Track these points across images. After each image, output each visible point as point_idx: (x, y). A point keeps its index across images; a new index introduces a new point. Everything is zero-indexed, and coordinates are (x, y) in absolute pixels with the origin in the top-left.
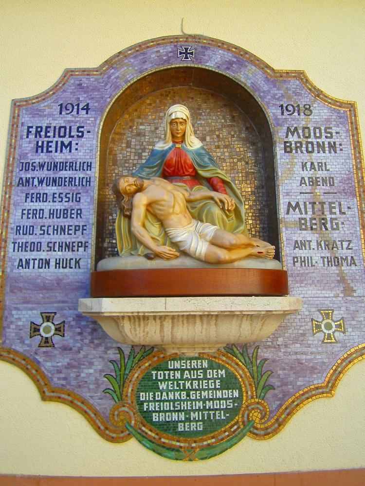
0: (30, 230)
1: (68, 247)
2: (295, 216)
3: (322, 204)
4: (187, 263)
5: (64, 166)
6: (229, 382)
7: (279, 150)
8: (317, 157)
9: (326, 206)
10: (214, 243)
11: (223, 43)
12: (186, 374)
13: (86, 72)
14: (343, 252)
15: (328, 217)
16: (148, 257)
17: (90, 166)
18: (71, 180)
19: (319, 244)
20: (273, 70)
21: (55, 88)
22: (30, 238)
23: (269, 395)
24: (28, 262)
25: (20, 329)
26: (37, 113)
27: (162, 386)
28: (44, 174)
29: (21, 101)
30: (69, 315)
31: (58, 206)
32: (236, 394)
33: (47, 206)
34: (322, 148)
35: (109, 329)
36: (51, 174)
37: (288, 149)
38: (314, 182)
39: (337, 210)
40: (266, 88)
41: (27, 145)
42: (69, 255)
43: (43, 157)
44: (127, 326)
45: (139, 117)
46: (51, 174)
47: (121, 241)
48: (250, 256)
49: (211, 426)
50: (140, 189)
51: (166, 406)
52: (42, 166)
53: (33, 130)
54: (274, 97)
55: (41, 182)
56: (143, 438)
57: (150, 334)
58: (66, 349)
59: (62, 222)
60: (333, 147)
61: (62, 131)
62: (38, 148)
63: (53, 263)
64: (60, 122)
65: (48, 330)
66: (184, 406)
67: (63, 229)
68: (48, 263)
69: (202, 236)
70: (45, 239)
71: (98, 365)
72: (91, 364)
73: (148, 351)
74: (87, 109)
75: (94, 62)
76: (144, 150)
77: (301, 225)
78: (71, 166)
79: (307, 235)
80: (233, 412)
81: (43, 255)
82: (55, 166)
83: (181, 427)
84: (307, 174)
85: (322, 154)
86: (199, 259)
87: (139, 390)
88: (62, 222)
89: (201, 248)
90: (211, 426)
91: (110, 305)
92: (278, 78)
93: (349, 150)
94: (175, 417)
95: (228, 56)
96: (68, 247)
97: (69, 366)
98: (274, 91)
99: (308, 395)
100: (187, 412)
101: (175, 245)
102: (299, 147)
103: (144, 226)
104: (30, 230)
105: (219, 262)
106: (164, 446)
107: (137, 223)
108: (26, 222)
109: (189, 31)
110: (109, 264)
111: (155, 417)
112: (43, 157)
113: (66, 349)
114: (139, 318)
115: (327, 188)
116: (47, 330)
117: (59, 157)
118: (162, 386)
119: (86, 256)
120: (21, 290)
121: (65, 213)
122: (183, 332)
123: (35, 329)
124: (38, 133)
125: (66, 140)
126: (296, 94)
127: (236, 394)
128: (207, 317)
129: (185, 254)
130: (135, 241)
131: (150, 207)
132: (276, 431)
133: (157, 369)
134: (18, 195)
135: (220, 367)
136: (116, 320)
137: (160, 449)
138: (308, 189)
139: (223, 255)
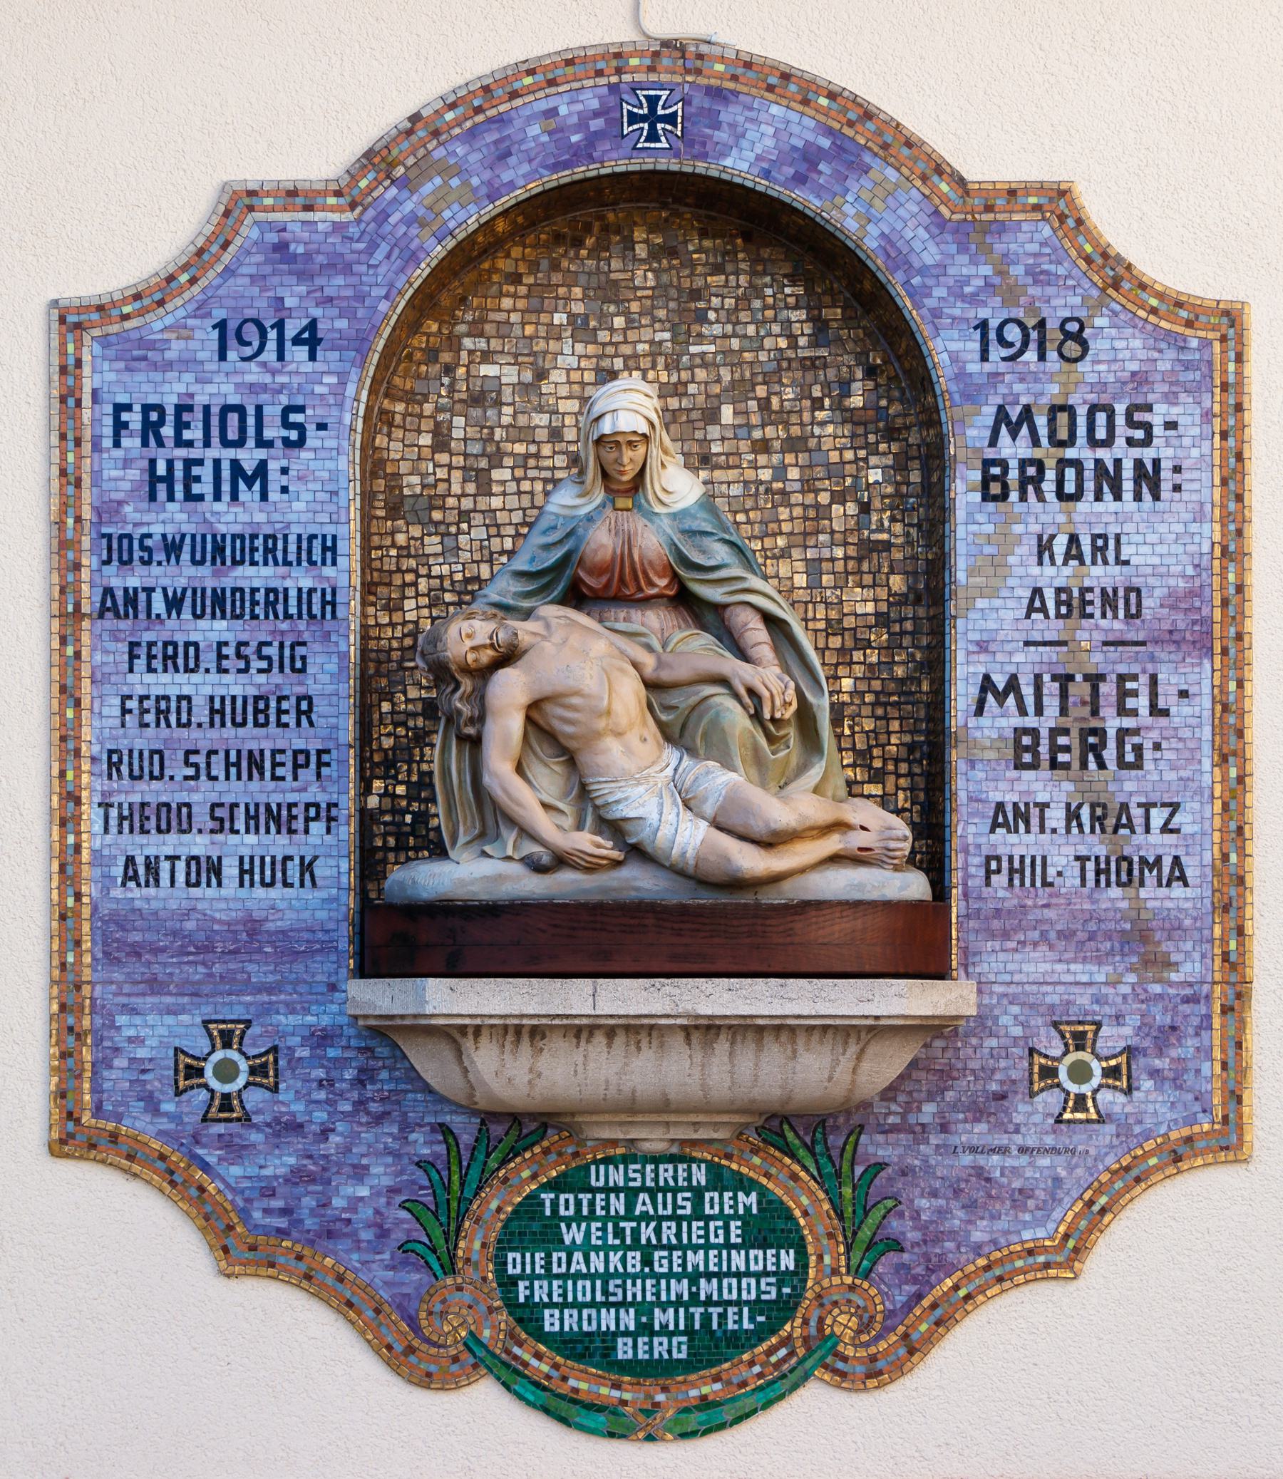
3: (1095, 680)
12: (643, 1204)
14: (1153, 843)
15: (1112, 724)
16: (538, 868)
17: (331, 549)
18: (274, 597)
19: (1072, 815)
20: (961, 182)
24: (152, 867)
27: (572, 1235)
28: (183, 575)
31: (235, 686)
32: (788, 1260)
34: (1109, 479)
36: (206, 577)
39: (1142, 703)
42: (279, 844)
45: (476, 330)
46: (206, 577)
50: (508, 656)
52: (172, 548)
53: (134, 419)
55: (174, 604)
59: (251, 738)
60: (1148, 478)
63: (230, 870)
67: (255, 762)
68: (215, 869)
70: (201, 796)
76: (496, 459)
81: (199, 844)
83: (624, 1350)
84: (1054, 575)
86: (678, 871)
88: (251, 738)
94: (608, 1320)
95: (804, 130)
97: (297, 1177)
98: (961, 266)
100: (644, 1309)
101: (614, 828)
102: (1031, 479)
103: (520, 770)
105: (737, 884)
106: (574, 1400)
108: (144, 741)
111: (551, 1321)
115: (1116, 626)
116: (226, 1071)
118: (572, 1235)
124: (150, 430)
125: (249, 457)
126: (1038, 276)
127: (788, 1260)
129: (638, 853)
132: (899, 1369)
133: (556, 1186)
135: (745, 1185)
139: (751, 861)
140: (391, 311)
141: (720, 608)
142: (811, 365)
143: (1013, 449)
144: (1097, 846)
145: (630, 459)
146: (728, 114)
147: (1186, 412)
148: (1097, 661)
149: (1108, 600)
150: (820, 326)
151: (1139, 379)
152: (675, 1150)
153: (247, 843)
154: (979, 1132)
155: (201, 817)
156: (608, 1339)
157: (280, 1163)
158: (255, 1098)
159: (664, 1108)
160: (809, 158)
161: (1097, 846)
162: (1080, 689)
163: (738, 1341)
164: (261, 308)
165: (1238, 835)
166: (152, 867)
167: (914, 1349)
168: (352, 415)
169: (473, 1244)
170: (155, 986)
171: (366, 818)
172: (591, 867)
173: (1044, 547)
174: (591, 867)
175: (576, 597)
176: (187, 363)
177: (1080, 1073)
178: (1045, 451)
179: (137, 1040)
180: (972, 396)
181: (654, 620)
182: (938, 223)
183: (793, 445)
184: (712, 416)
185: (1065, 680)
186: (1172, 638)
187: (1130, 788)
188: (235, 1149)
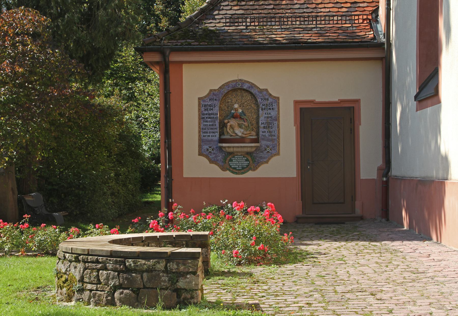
0: (205, 129)
1: (214, 133)
2: (263, 125)
3: (269, 123)
4: (238, 137)
5: (211, 114)
6: (247, 160)
7: (260, 110)
8: (269, 111)
9: (270, 123)
10: (243, 133)
11: (248, 82)
12: (238, 159)
13: (215, 90)
14: (273, 134)
15: (270, 126)
16: (230, 136)
17: (217, 114)
18: (213, 117)
19: (268, 132)
20: (260, 89)
21: (208, 94)
22: (205, 131)
23: (255, 163)
24: (205, 136)
25: (204, 149)
26: (204, 101)
27: (234, 161)
28: (207, 116)
29: (200, 98)
30: (215, 147)
31: (211, 124)
32: (248, 162)
33: (208, 124)
34: (270, 109)
35: (224, 149)
36: (209, 116)
37: (262, 110)
38: (268, 117)
39: (272, 124)
40: (258, 94)
41: (203, 109)
42: (214, 134)
43: (206, 112)
44: (227, 149)
45: (228, 98)
46: (209, 116)
47: (226, 133)
48: (250, 136)
49: (243, 168)
50: (229, 122)
51: (234, 164)
52: (206, 114)
53: (204, 105)
54: (260, 96)
55: (207, 118)
56: (230, 170)
57: (231, 150)
58: (214, 153)
59: (212, 127)
60: (273, 109)
61: (210, 106)
62: (205, 110)
63: (210, 136)
64: (210, 103)
65: (210, 150)
66: (238, 164)
67: (212, 129)
68: (209, 136)
69: (241, 132)
70: (208, 131)
71: (221, 157)
72: (219, 157)
73: (230, 153)
74: (216, 100)
75: (217, 88)
76: (229, 107)
77: (264, 127)
78: (213, 114)
79: (265, 130)
80: (247, 166)
81: (208, 134)
82: (209, 114)
83: (237, 169)
84: (266, 115)
85: (270, 111)
86: (240, 136)
87: (229, 161)
88: (212, 127)
89: (240, 134)
90: (243, 168)
91: (224, 145)
92: (261, 91)
93: (277, 109)
94: (236, 166)
95: (249, 85)
96: (214, 133)
97: (215, 157)
98: (260, 95)
99: (262, 163)
100: (238, 166)
101: (236, 134)
102: (265, 109)
103: (229, 130)
104: (205, 129)
105: (243, 137)
106: (234, 172)
107: (228, 130)
108: (205, 127)
109: (240, 78)
110: (223, 137)
111: (232, 167)
112: (206, 112)
113: (214, 153)
114: (229, 147)
115: (270, 119)
116: (210, 150)
117: (210, 112)
118: (234, 161)
119: (217, 135)
120: (204, 142)
121: (212, 125)
122: (235, 150)
123: (208, 150)
124: (205, 106)
125: (212, 108)
126: (265, 95)
127: (248, 162)
128: (241, 147)
129: (237, 135)
130: (228, 133)
131: (231, 126)
132: (256, 170)
133: (233, 157)
134: (202, 121)
135: (245, 157)
136: (225, 147)
137: (233, 172)
138: (266, 119)
139: (244, 136)
140: (221, 98)
141: (243, 119)
142: (251, 100)
143: (263, 107)
144: (269, 134)
145: (236, 109)
146: (244, 84)
147: (275, 104)
148: (269, 121)
149: (270, 117)
150: (252, 98)
151: (272, 102)
152: (423, 272)
153: (212, 134)
154: (262, 153)
155: (208, 132)
156: (236, 168)
157: (214, 156)
158: (212, 151)
159: (239, 152)
160: (250, 87)
161: (269, 134)
162: (268, 123)
163: (245, 168)
164: (212, 98)
165: (279, 133)
166: (205, 136)
167: (257, 168)
168: (219, 105)
169: (227, 161)
170: (205, 144)
171: (220, 132)
172: (234, 136)
173: (266, 114)
174: (234, 136)
175: (234, 118)
176: (207, 102)
177: (268, 149)
178: (266, 107)
179: (116, 212)
180: (261, 103)
181: (238, 119)
182: (258, 91)
183: (250, 106)
184: (244, 103)
185: (267, 123)
186: (274, 120)
187: (271, 130)
188: (211, 155)
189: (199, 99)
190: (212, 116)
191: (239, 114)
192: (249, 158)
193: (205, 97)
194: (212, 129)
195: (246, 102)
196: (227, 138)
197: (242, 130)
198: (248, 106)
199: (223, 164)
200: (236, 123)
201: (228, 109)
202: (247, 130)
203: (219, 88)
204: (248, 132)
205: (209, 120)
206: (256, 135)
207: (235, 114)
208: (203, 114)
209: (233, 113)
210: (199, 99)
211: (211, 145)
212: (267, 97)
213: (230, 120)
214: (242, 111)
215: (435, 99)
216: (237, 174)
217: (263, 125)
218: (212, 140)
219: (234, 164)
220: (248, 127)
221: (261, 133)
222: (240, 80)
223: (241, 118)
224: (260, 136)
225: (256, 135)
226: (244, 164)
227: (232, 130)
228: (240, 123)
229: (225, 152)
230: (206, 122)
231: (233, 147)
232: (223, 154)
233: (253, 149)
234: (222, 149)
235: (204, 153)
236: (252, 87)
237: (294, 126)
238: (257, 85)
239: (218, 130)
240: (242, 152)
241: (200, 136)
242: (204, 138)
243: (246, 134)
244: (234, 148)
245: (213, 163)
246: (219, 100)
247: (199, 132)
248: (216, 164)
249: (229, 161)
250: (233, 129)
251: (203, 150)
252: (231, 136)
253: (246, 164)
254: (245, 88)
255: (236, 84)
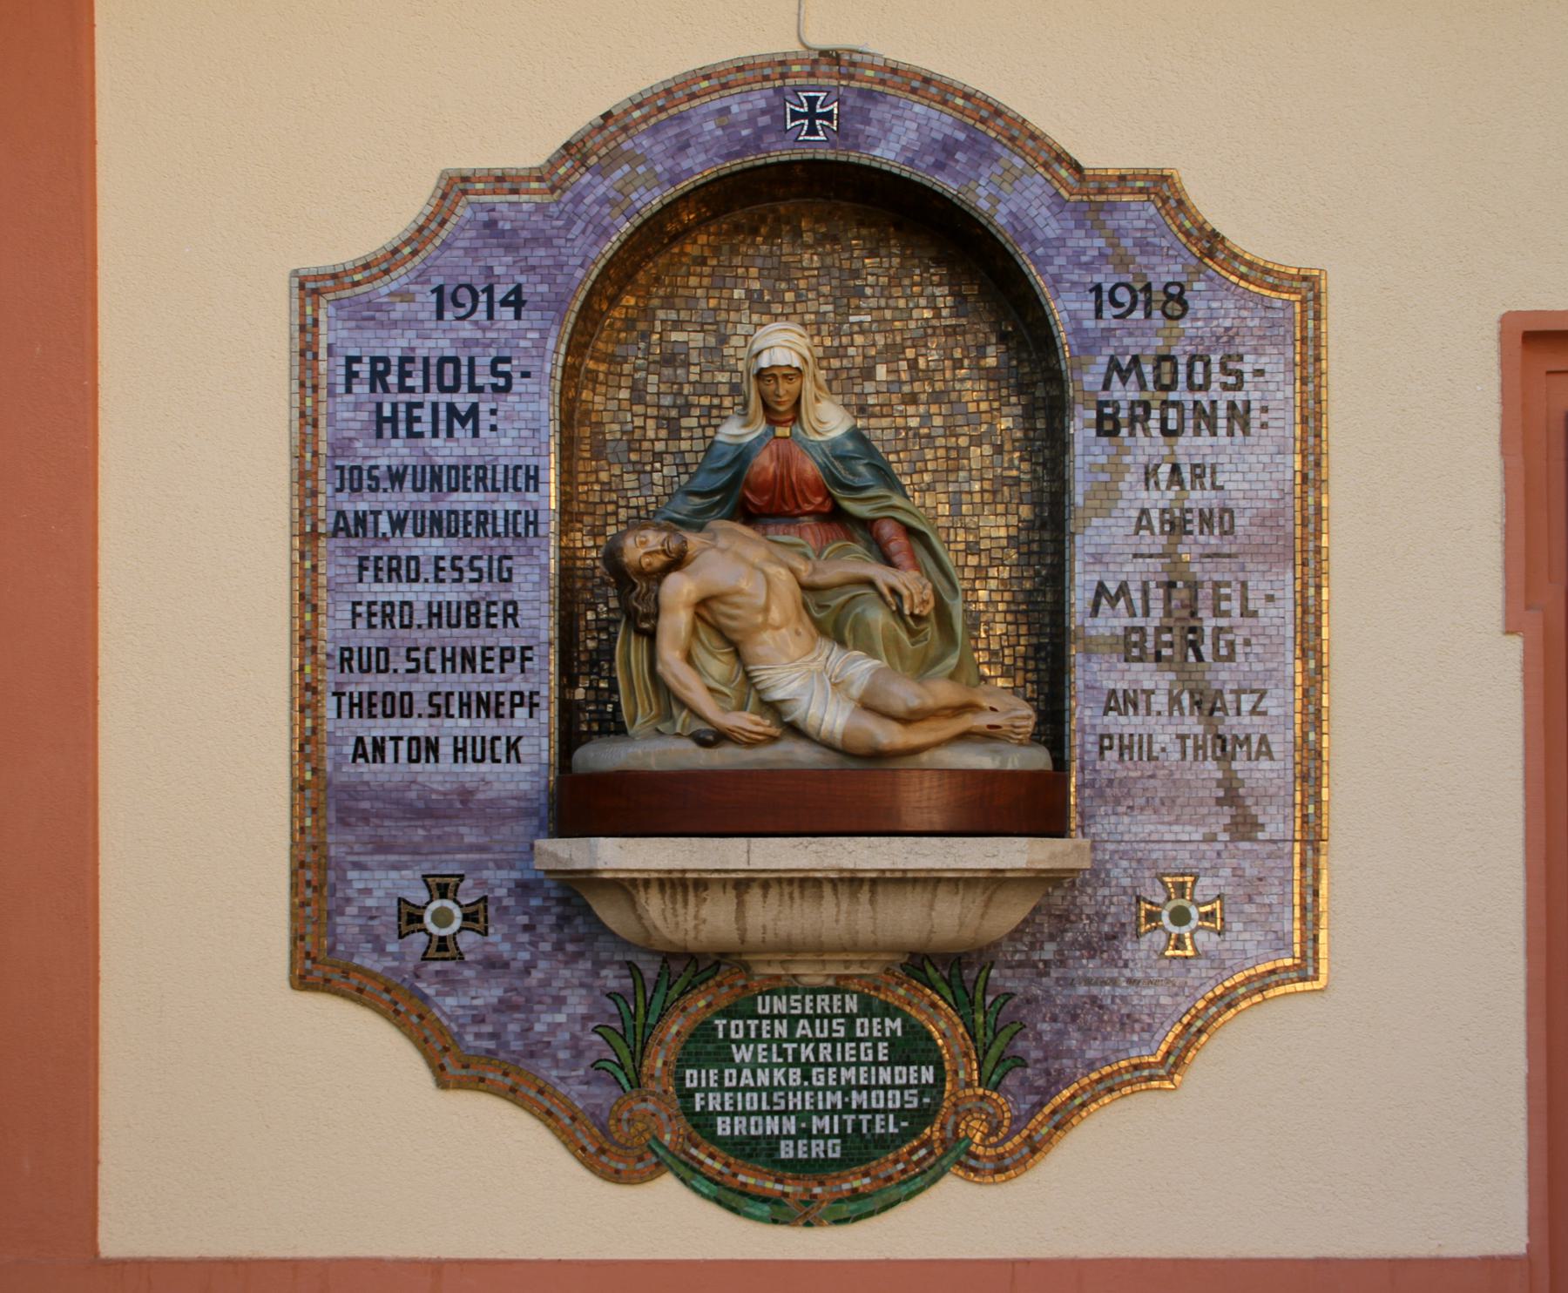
0: (377, 661)
1: (487, 705)
4: (800, 754)
7: (1080, 427)
8: (1192, 446)
9: (1206, 592)
10: (868, 706)
12: (803, 1028)
13: (503, 181)
16: (702, 742)
17: (534, 479)
19: (1174, 701)
20: (1077, 168)
21: (420, 235)
22: (380, 683)
24: (379, 746)
25: (369, 914)
26: (368, 315)
27: (742, 1054)
28: (404, 500)
30: (500, 881)
31: (451, 593)
32: (928, 1075)
33: (420, 594)
34: (1205, 418)
35: (611, 914)
36: (425, 501)
37: (1107, 425)
39: (1235, 607)
42: (487, 726)
43: (396, 452)
44: (654, 906)
45: (668, 302)
46: (425, 501)
47: (639, 709)
48: (965, 737)
50: (677, 561)
51: (751, 1101)
52: (397, 477)
53: (363, 369)
54: (1076, 261)
55: (398, 524)
56: (690, 1173)
58: (493, 965)
59: (464, 637)
63: (446, 749)
64: (438, 344)
66: (795, 1101)
68: (433, 747)
70: (421, 686)
71: (577, 1004)
72: (559, 1002)
74: (516, 301)
76: (685, 409)
77: (1130, 646)
78: (482, 477)
81: (419, 727)
82: (435, 478)
83: (786, 1151)
85: (1205, 439)
86: (827, 745)
87: (683, 1064)
88: (464, 637)
93: (1285, 424)
94: (772, 1125)
95: (943, 124)
96: (487, 705)
97: (505, 1006)
98: (1078, 239)
100: (803, 1116)
101: (773, 709)
103: (689, 658)
104: (377, 661)
105: (878, 756)
106: (743, 1192)
109: (821, 38)
111: (723, 1127)
112: (396, 452)
113: (493, 965)
114: (678, 885)
116: (443, 918)
117: (447, 451)
118: (742, 1054)
120: (365, 817)
124: (378, 378)
125: (463, 400)
126: (1143, 246)
127: (928, 1075)
128: (851, 882)
129: (795, 730)
130: (667, 697)
131: (704, 608)
132: (1022, 1164)
133: (728, 1014)
135: (889, 1011)
136: (626, 887)
137: (732, 1198)
139: (889, 735)
141: (867, 525)
142: (951, 331)
146: (878, 112)
149: (1206, 520)
151: (1230, 335)
153: (461, 726)
154: (1091, 966)
155: (421, 704)
156: (773, 1141)
157: (491, 994)
158: (468, 940)
159: (819, 950)
160: (948, 148)
163: (885, 1143)
165: (1314, 718)
166: (379, 746)
167: (1035, 1148)
169: (657, 1062)
170: (382, 847)
172: (751, 744)
175: (748, 515)
176: (409, 322)
180: (1088, 347)
181: (807, 535)
182: (1059, 203)
183: (936, 397)
184: (868, 374)
188: (449, 983)
189: (309, 288)
190: (468, 500)
191: (810, 468)
192: (943, 1027)
193: (389, 260)
194: (468, 658)
195: (892, 353)
196: (653, 764)
197: (861, 669)
198: (912, 399)
199: (603, 1095)
200: (781, 575)
201: (674, 433)
202: (923, 668)
203: (553, 164)
204: (942, 692)
205: (432, 546)
206: (1036, 738)
207: (765, 462)
208: (354, 479)
209: (742, 456)
210: (309, 288)
211: (449, 866)
212: (1163, 273)
213: (694, 540)
214: (855, 434)
215: (784, 707)
216: (779, 1212)
217: (1112, 622)
218: (464, 802)
219: (751, 1101)
220: (931, 629)
221: (1084, 715)
222: (831, 57)
223: (835, 517)
224: (1080, 744)
225: (1036, 738)
226: (878, 1100)
227: (718, 666)
228: (833, 572)
229: (627, 945)
230: (395, 569)
231: (741, 884)
232: (612, 978)
233: (1009, 914)
234: (587, 911)
235: (370, 962)
236: (980, 149)
237: (1509, 631)
238: (1039, 120)
239: (544, 676)
240: (849, 948)
241: (307, 745)
242: (367, 770)
243: (908, 719)
244: (754, 896)
245: (478, 1084)
246: (557, 304)
247: (306, 695)
248: (512, 1094)
249: (683, 1064)
250: (736, 649)
251: (348, 924)
252: (717, 738)
253: (895, 1100)
254: (887, 153)
255: (774, 111)
